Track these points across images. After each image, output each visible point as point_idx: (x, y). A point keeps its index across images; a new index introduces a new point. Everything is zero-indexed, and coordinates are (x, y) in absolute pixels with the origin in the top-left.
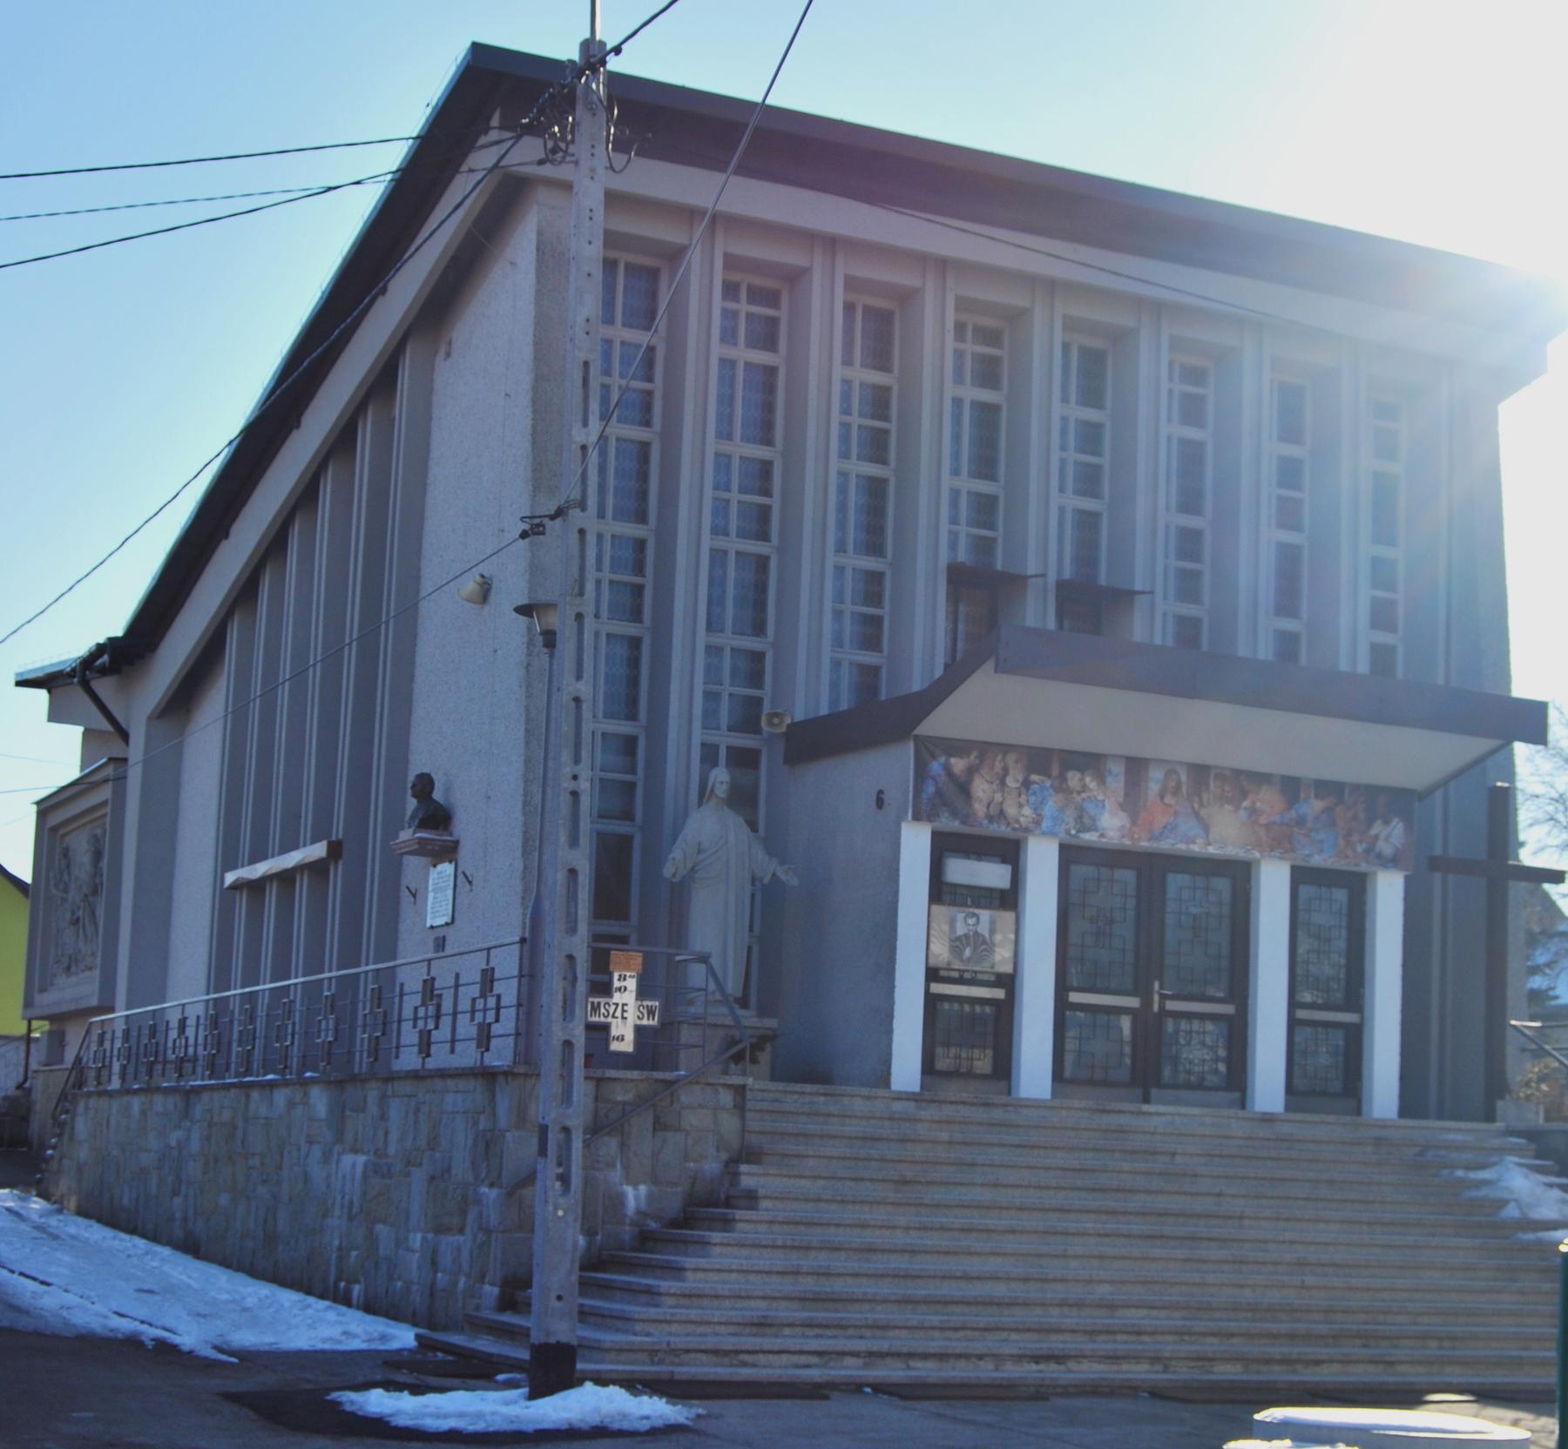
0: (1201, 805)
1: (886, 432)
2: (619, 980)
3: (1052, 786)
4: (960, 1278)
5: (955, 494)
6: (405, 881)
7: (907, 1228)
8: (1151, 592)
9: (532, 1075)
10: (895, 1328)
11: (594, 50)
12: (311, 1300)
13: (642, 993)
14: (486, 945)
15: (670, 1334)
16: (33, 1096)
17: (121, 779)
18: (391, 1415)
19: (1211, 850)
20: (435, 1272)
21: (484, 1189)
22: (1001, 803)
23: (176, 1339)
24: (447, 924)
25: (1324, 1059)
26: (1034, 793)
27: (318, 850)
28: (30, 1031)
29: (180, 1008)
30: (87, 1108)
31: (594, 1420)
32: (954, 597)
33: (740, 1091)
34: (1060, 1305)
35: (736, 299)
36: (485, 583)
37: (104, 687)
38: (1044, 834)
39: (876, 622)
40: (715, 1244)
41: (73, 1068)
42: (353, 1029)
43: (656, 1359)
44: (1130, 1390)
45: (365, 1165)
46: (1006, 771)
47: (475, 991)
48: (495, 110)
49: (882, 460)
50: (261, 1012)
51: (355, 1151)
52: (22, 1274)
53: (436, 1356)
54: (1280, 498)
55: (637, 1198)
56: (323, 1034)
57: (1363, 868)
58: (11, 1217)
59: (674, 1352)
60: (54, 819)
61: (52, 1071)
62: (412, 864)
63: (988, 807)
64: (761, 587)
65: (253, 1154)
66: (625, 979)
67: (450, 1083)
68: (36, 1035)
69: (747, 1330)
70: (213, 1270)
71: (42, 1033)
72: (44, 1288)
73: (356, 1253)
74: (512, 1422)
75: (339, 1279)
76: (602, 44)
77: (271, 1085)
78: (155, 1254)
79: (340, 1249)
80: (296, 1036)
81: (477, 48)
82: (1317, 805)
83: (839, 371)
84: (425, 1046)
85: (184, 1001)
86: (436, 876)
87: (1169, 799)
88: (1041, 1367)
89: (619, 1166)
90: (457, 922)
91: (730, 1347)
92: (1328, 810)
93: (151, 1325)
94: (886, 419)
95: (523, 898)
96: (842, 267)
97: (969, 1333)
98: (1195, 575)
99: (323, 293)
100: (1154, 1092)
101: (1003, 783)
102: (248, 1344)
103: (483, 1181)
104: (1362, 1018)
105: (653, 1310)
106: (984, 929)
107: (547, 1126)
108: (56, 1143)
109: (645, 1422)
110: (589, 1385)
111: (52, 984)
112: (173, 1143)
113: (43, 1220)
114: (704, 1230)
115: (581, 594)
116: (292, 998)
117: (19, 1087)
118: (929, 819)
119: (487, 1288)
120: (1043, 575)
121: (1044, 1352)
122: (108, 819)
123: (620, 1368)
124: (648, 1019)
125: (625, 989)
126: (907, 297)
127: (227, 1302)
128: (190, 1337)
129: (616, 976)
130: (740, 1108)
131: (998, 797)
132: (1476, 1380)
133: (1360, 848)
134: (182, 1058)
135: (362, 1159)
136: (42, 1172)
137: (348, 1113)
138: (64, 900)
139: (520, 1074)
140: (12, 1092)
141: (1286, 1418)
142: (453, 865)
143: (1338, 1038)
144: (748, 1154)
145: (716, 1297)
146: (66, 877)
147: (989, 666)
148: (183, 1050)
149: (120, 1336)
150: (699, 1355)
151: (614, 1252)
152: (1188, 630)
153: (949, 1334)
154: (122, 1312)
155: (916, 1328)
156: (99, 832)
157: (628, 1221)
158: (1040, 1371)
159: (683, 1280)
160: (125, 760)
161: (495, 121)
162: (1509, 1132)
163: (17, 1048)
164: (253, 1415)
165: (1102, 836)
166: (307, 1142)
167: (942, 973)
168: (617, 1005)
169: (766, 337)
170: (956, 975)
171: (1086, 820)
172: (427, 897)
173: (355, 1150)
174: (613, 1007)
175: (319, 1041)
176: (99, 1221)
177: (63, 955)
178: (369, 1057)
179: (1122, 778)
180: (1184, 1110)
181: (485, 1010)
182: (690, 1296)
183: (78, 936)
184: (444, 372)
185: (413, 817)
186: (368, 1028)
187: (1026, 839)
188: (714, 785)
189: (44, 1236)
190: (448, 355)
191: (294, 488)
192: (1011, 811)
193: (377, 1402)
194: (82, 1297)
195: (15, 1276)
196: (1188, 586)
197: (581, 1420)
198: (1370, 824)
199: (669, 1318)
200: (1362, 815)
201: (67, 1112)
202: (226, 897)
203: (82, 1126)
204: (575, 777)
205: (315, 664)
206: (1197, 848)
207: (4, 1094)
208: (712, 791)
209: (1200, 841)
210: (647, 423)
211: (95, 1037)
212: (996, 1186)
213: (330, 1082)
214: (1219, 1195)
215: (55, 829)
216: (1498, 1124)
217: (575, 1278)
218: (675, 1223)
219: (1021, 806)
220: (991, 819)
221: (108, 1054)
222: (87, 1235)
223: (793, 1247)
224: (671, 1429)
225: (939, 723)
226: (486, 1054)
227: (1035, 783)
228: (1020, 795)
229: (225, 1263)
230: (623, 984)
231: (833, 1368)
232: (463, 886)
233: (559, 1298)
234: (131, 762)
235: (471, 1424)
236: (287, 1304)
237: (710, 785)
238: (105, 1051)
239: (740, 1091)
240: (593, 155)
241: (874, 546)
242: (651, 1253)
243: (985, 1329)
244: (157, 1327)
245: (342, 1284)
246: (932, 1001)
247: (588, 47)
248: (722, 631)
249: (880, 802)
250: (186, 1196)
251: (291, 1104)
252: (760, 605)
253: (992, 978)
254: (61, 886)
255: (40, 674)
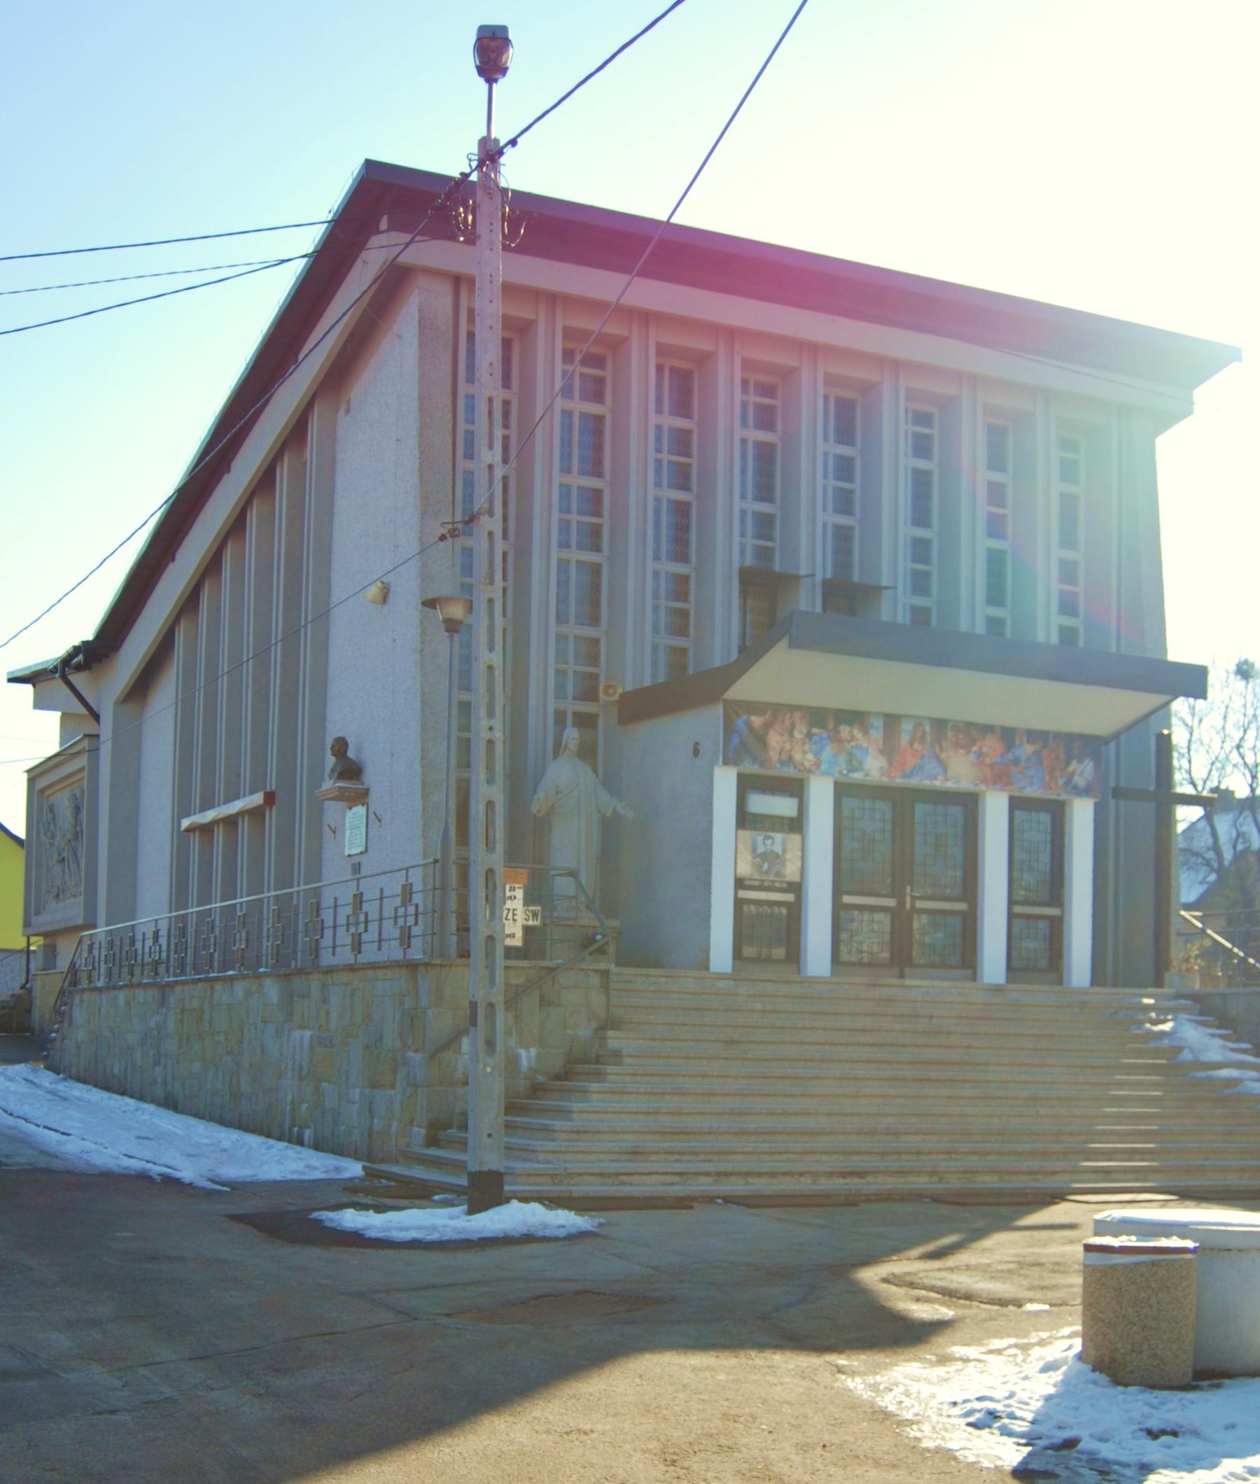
0: (941, 748)
1: (851, 492)
2: (510, 890)
3: (829, 737)
4: (781, 1114)
5: (743, 513)
6: (326, 821)
7: (737, 1077)
8: (895, 588)
9: (446, 965)
10: (734, 1153)
11: (491, 146)
12: (272, 1142)
13: (527, 902)
14: (406, 865)
15: (565, 1162)
16: (34, 994)
17: (94, 751)
18: (365, 1229)
19: (950, 785)
20: (372, 1118)
21: (411, 1054)
22: (790, 751)
23: (178, 1175)
24: (362, 853)
25: (1033, 945)
26: (815, 743)
27: (257, 799)
28: (29, 945)
29: (154, 922)
30: (82, 1001)
31: (524, 1230)
32: (744, 594)
33: (605, 974)
34: (858, 1133)
35: (572, 362)
36: (385, 588)
37: (78, 679)
38: (823, 774)
39: (684, 614)
40: (593, 1092)
41: (68, 972)
42: (259, 939)
43: (556, 1181)
44: (917, 1197)
45: (312, 1037)
46: (793, 726)
47: (349, 910)
48: (381, 217)
49: (685, 487)
50: (191, 929)
51: (302, 1027)
52: (45, 1127)
53: (381, 1183)
54: (990, 514)
55: (529, 1059)
56: (237, 944)
57: (1063, 797)
58: (28, 1085)
59: (570, 1175)
60: (42, 783)
61: (47, 974)
62: (332, 808)
63: (780, 753)
64: (596, 588)
65: (219, 1032)
66: (514, 890)
67: (380, 973)
68: (32, 948)
69: (624, 1157)
70: (192, 1121)
71: (39, 946)
72: (65, 1137)
73: (306, 1105)
74: (460, 1232)
75: (292, 1125)
76: (497, 141)
77: (231, 979)
78: (144, 1110)
79: (293, 1103)
80: (217, 946)
81: (370, 165)
82: (1029, 749)
83: (653, 419)
84: (357, 946)
85: (157, 917)
86: (351, 816)
87: (917, 746)
88: (847, 1180)
89: (514, 1032)
90: (369, 851)
91: (613, 1171)
92: (1037, 753)
93: (155, 1164)
94: (688, 455)
95: (424, 831)
96: (654, 336)
97: (792, 1156)
98: (926, 575)
99: (248, 365)
100: (907, 970)
101: (791, 735)
102: (234, 1176)
103: (409, 1047)
104: (1063, 912)
105: (551, 1144)
106: (778, 848)
107: (476, 1003)
108: (58, 1028)
109: (562, 1230)
110: (515, 1203)
111: (44, 909)
112: (153, 1025)
113: (52, 1086)
114: (584, 1082)
115: (492, 583)
116: (213, 918)
117: (23, 987)
118: (736, 764)
119: (416, 1129)
120: (813, 575)
121: (849, 1170)
122: (86, 779)
123: (531, 1188)
124: (533, 920)
125: (515, 898)
126: (704, 359)
127: (208, 1145)
128: (187, 1172)
129: (508, 887)
130: (606, 987)
131: (788, 746)
132: (1174, 1183)
133: (1061, 782)
134: (157, 961)
135: (308, 1033)
136: (48, 1050)
137: (295, 999)
138: (52, 845)
139: (437, 965)
140: (18, 991)
141: (1123, 1217)
142: (365, 807)
143: (1043, 926)
144: (610, 1023)
145: (598, 1132)
146: (52, 828)
147: (784, 643)
148: (157, 954)
149: (132, 1173)
150: (589, 1178)
151: (513, 1100)
152: (921, 616)
153: (776, 1157)
154: (131, 1154)
155: (752, 1153)
156: (78, 792)
157: (522, 1075)
158: (846, 1184)
159: (571, 1121)
160: (97, 736)
161: (384, 224)
162: (1178, 996)
163: (21, 957)
164: (255, 1231)
165: (867, 775)
166: (262, 1022)
167: (747, 883)
168: (509, 910)
169: (596, 391)
170: (757, 883)
171: (855, 763)
172: (344, 833)
173: (302, 1027)
174: (506, 912)
175: (234, 948)
176: (96, 1086)
177: (52, 887)
178: (272, 959)
179: (882, 731)
180: (937, 983)
181: (406, 916)
182: (578, 1132)
183: (64, 872)
184: (343, 422)
185: (333, 771)
186: (271, 939)
187: (809, 778)
188: (567, 742)
189: (56, 1098)
190: (348, 411)
191: (226, 522)
192: (798, 756)
193: (351, 1219)
194: (96, 1144)
195: (41, 1129)
196: (920, 583)
197: (514, 1230)
198: (1068, 763)
199: (563, 1149)
200: (1062, 756)
201: (66, 1004)
202: (182, 838)
203: (79, 1015)
204: (491, 729)
205: (248, 661)
206: (939, 783)
207: (11, 992)
208: (566, 746)
209: (941, 778)
210: (599, 475)
211: (85, 947)
212: (801, 1043)
213: (279, 976)
214: (969, 1047)
215: (42, 791)
216: (1165, 990)
217: (502, 1119)
218: (558, 1077)
219: (805, 752)
220: (782, 763)
221: (97, 959)
222: (89, 1097)
223: (652, 1094)
224: (582, 1235)
225: (740, 690)
226: (408, 950)
227: (815, 735)
228: (804, 744)
229: (198, 1115)
230: (513, 893)
231: (691, 1185)
232: (374, 823)
233: (490, 1135)
234: (103, 738)
235: (428, 1235)
236: (255, 1145)
237: (564, 742)
238: (94, 958)
239: (605, 974)
240: (491, 231)
241: (680, 554)
242: (541, 1100)
243: (802, 1153)
244: (160, 1165)
245: (296, 1129)
246: (739, 903)
247: (486, 143)
248: (567, 623)
249: (696, 752)
250: (165, 1066)
251: (248, 994)
252: (596, 604)
253: (785, 885)
254: (49, 834)
255: (27, 672)
